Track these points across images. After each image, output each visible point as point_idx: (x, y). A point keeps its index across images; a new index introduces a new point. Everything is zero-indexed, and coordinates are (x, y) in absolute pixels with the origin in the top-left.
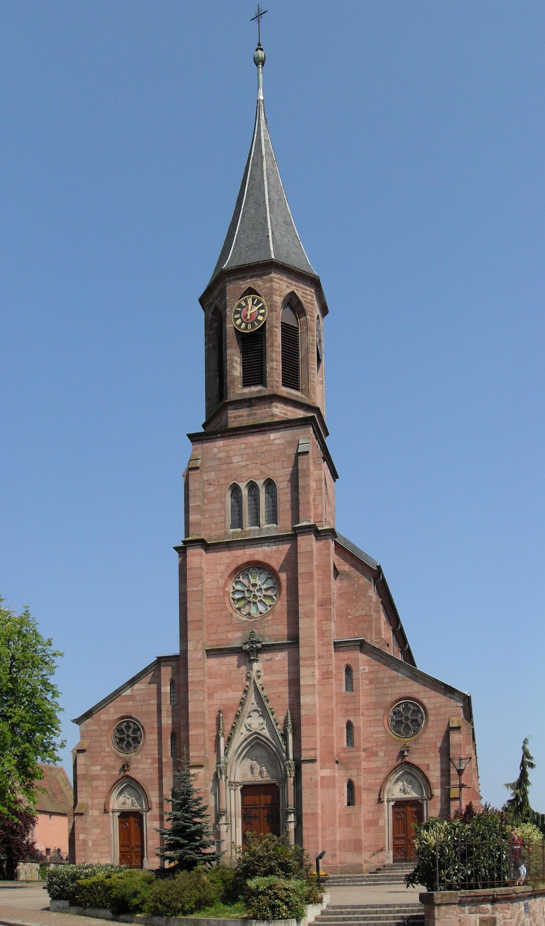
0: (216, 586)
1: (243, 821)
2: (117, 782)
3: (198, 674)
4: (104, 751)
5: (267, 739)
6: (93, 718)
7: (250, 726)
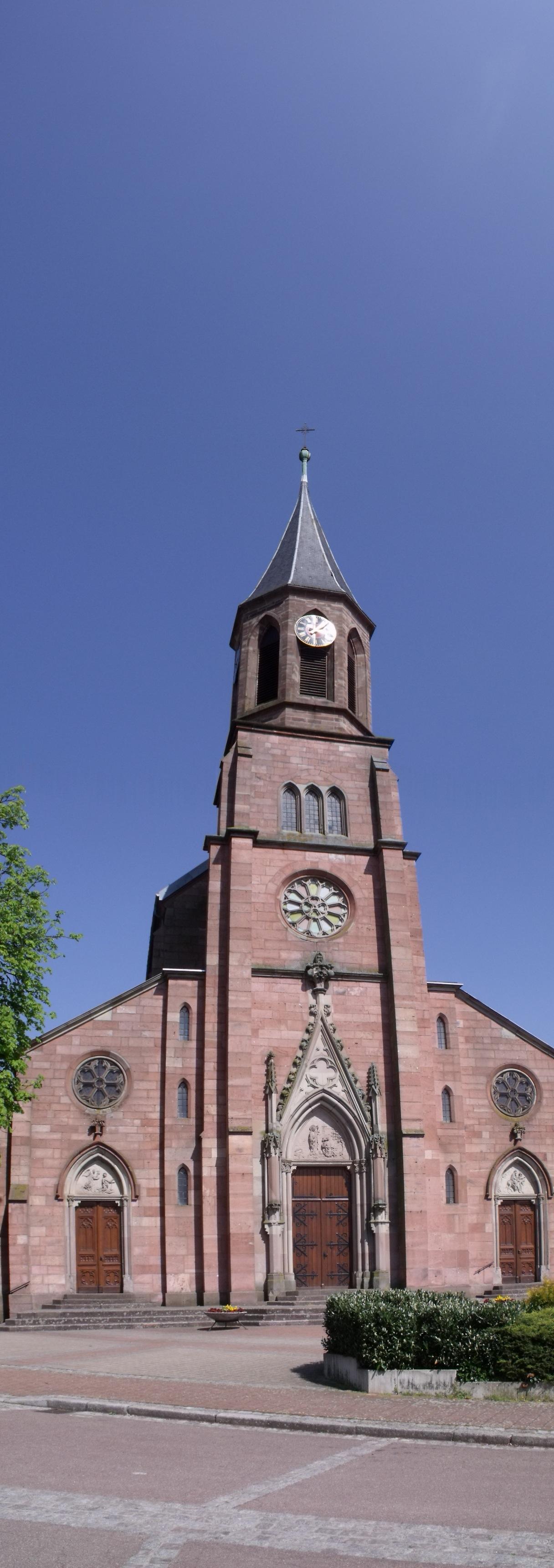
0: (264, 891)
1: (294, 1221)
2: (80, 1153)
3: (244, 999)
4: (59, 1103)
5: (340, 1101)
6: (42, 1050)
7: (314, 1080)
